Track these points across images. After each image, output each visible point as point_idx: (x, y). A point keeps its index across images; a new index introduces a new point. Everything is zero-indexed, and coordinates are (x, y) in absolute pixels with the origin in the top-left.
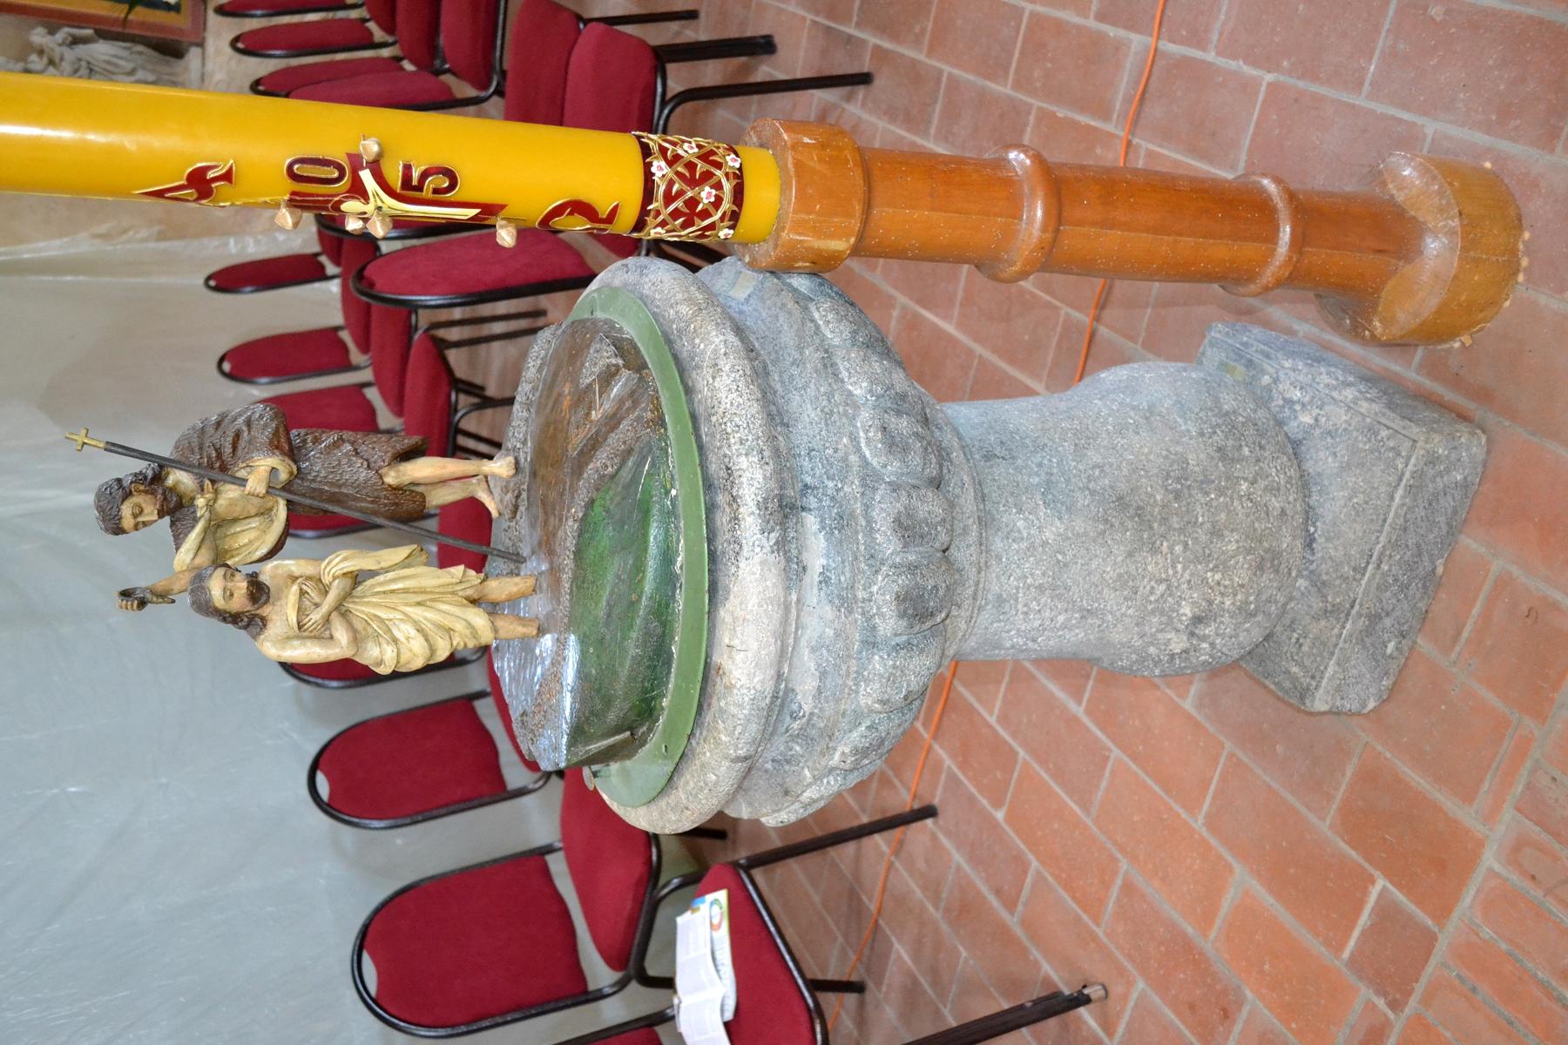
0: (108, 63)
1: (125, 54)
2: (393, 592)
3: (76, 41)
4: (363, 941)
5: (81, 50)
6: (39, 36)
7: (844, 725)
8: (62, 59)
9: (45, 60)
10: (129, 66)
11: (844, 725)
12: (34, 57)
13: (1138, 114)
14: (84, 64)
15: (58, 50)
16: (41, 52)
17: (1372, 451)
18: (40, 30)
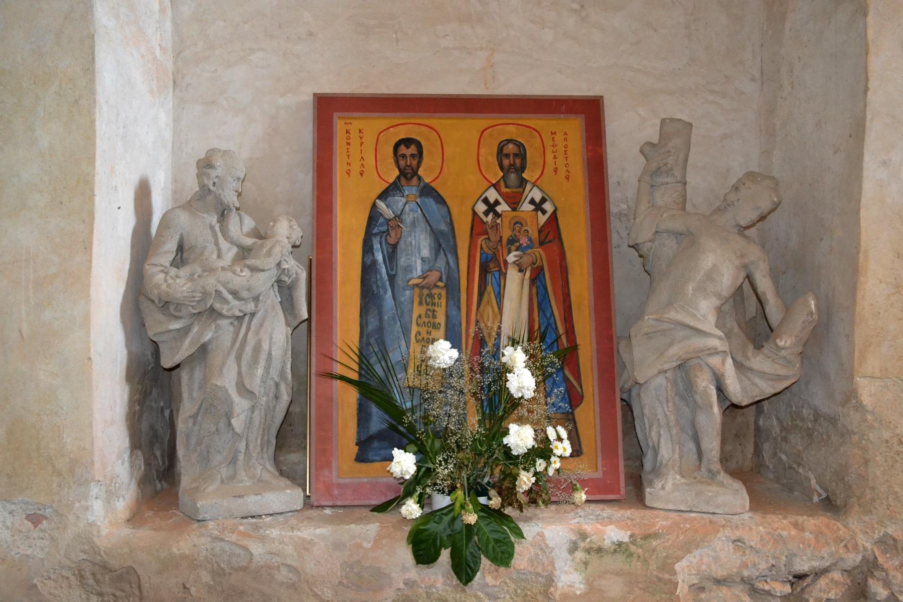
0: (257, 349)
1: (274, 374)
2: (596, 452)
3: (285, 289)
4: (582, 397)
5: (273, 298)
6: (288, 231)
7: (561, 411)
8: (254, 269)
9: (249, 241)
10: (255, 384)
11: (561, 411)
12: (249, 223)
13: (318, 507)
14: (251, 307)
15: (271, 263)
16: (260, 235)
17: (547, 366)
18: (297, 234)
